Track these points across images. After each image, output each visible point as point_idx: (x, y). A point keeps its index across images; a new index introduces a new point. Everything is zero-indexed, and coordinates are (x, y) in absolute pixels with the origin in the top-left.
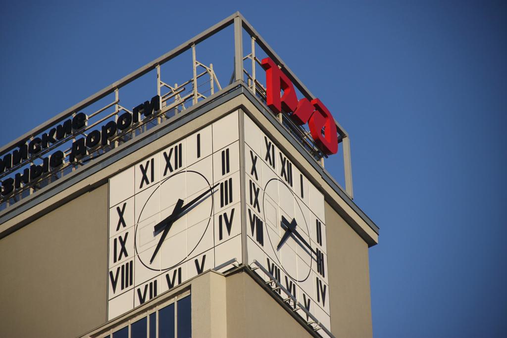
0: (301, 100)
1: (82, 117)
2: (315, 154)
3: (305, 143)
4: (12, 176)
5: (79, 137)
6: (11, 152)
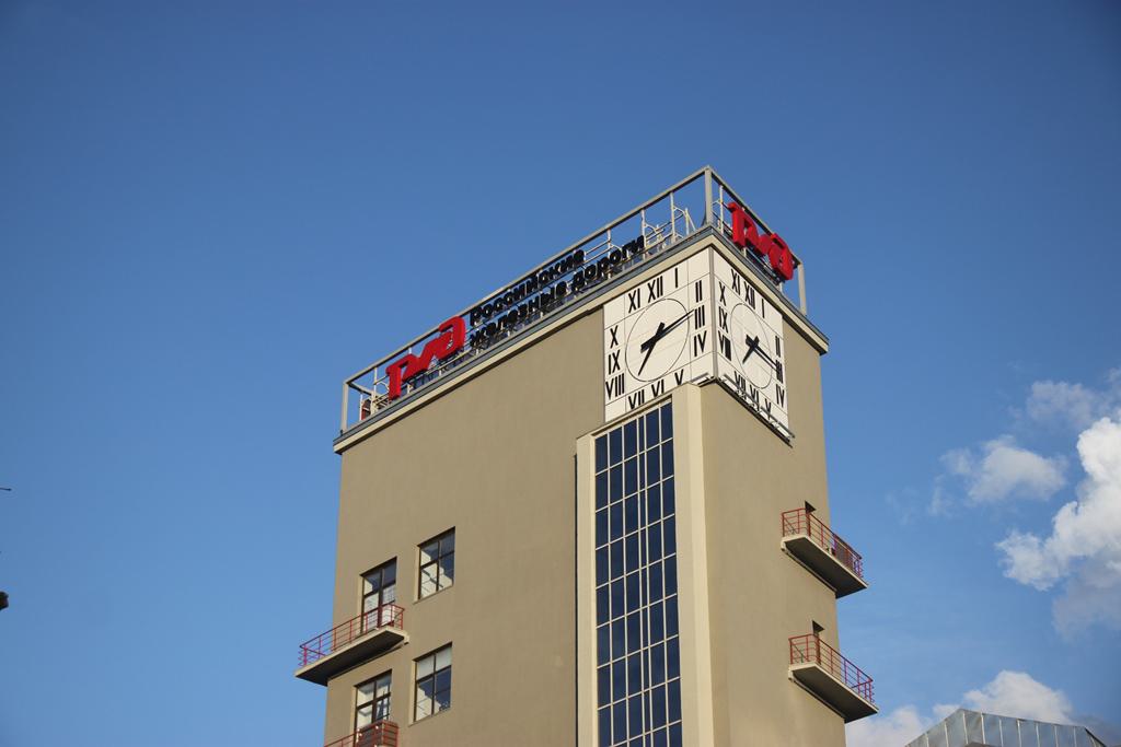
0: (763, 236)
1: (581, 253)
2: (774, 279)
3: (765, 272)
4: (525, 302)
5: (579, 270)
6: (525, 282)
